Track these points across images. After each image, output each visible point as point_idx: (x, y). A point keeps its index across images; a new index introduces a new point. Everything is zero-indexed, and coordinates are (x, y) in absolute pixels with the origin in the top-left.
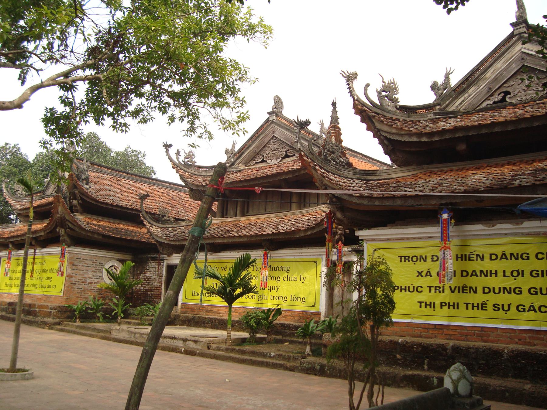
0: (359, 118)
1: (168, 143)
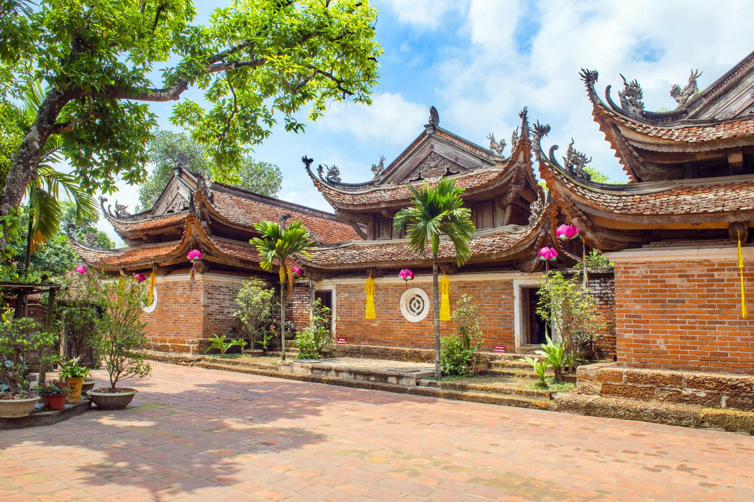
0: (598, 125)
1: (309, 158)
